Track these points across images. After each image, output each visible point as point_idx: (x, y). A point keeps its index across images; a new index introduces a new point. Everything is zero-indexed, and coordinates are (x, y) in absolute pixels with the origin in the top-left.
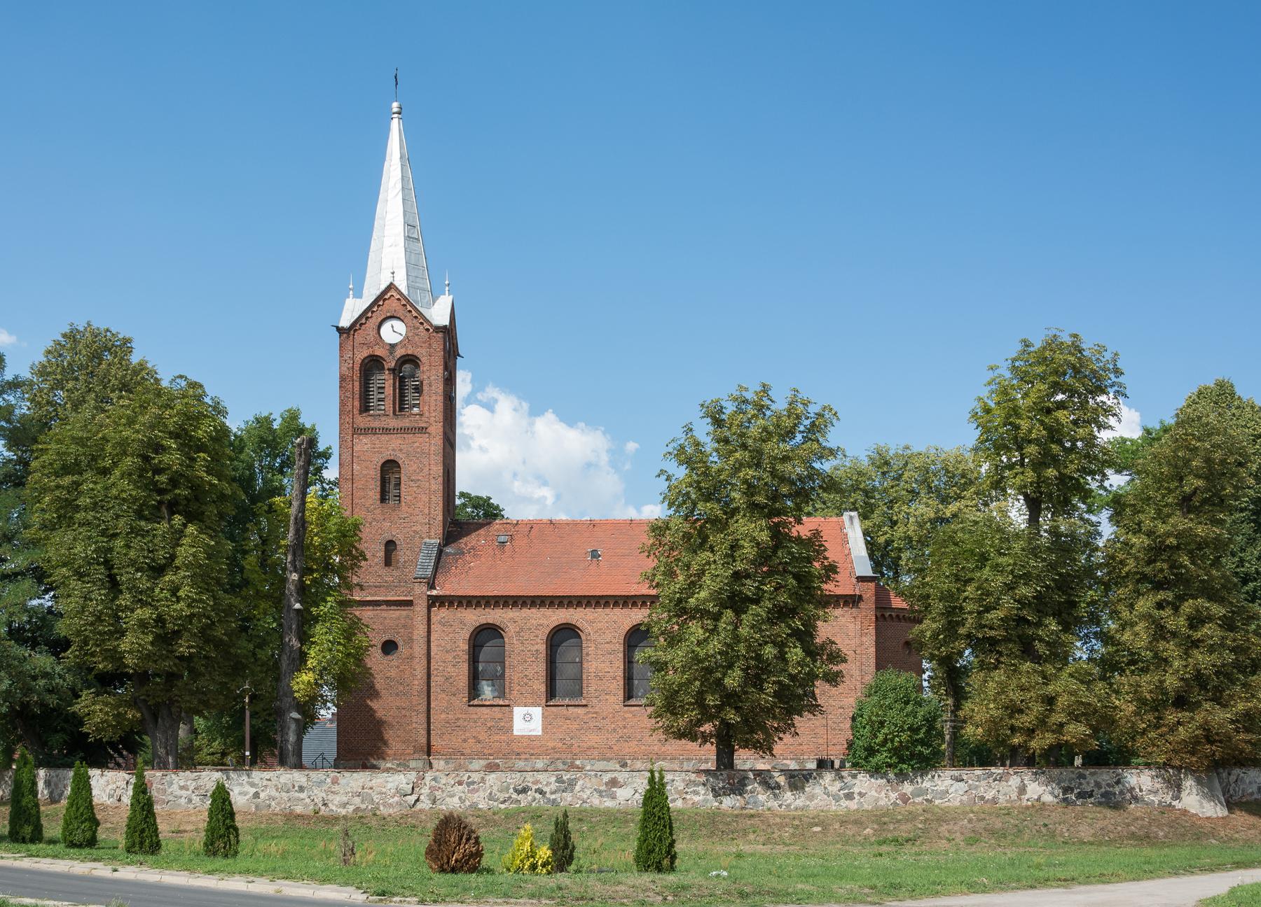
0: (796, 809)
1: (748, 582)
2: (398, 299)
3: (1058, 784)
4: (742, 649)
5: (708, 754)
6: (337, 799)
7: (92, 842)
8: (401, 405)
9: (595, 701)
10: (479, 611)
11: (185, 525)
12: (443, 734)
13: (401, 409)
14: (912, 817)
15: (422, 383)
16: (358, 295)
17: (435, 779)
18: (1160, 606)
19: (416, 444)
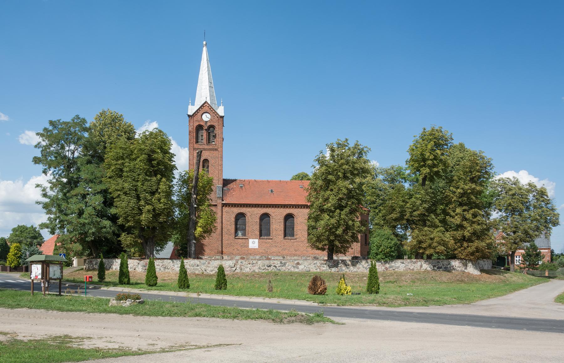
0: (354, 272)
1: (343, 201)
2: (208, 107)
3: (432, 265)
4: (342, 222)
5: (324, 255)
6: (209, 269)
7: (155, 284)
8: (209, 141)
10: (238, 208)
11: (161, 179)
12: (227, 247)
13: (209, 143)
14: (392, 275)
15: (216, 134)
16: (193, 104)
17: (241, 262)
18: (464, 210)
19: (214, 154)
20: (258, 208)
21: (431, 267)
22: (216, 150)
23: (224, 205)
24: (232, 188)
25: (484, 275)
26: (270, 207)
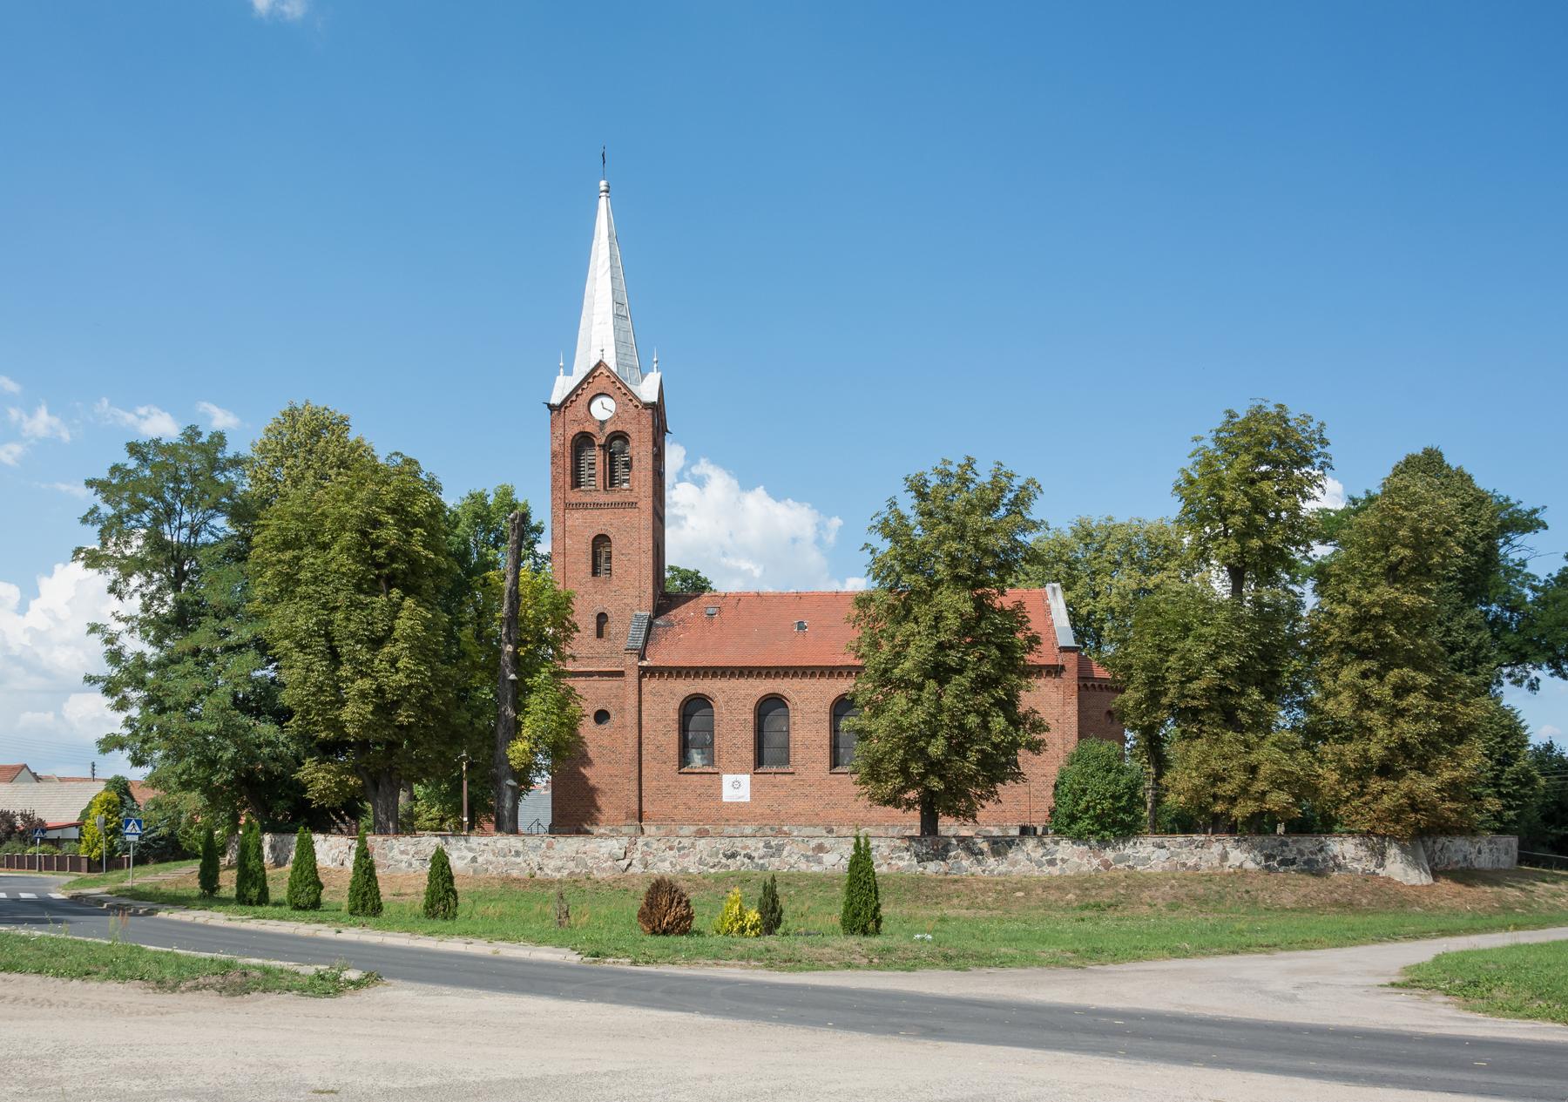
2: (608, 377)
4: (945, 718)
5: (912, 821)
6: (552, 864)
7: (316, 905)
8: (611, 481)
9: (802, 769)
10: (689, 681)
13: (612, 485)
15: (631, 458)
16: (569, 372)
17: (646, 844)
18: (1365, 675)
20: (750, 680)
21: (1258, 859)
23: (645, 672)
24: (682, 620)
25: (1446, 886)
26: (786, 675)
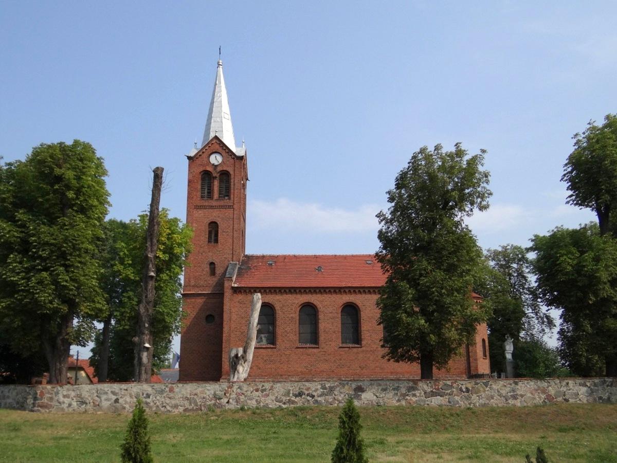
19: (227, 214)
22: (230, 207)
26: (315, 292)
